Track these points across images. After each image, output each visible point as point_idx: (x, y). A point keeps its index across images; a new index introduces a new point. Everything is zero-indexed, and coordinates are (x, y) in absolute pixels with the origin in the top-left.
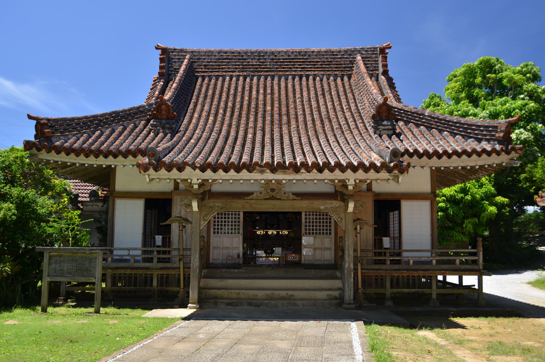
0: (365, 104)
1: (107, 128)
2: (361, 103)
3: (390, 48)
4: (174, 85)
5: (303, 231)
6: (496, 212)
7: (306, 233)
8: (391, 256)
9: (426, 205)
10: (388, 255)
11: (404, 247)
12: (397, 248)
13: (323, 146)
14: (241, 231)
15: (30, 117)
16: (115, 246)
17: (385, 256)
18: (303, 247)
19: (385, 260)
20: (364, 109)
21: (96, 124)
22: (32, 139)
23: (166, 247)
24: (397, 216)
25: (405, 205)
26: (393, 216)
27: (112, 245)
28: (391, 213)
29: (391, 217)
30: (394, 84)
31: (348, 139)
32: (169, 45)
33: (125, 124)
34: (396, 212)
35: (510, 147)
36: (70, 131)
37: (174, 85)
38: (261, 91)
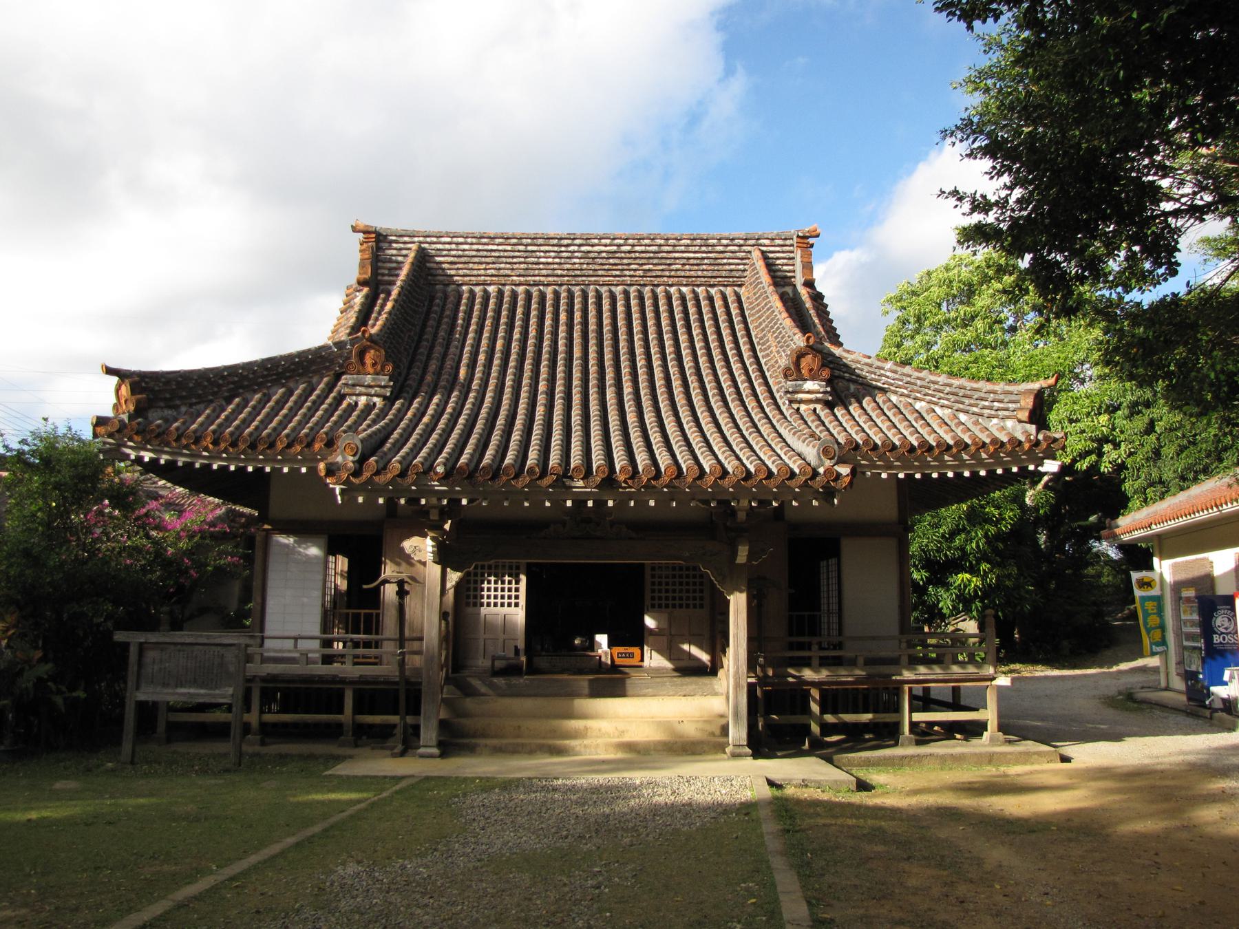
0: (769, 347)
1: (255, 392)
2: (764, 344)
3: (817, 236)
4: (389, 305)
5: (648, 602)
6: (63, 710)
7: (653, 606)
8: (821, 648)
9: (275, 511)
10: (815, 647)
11: (848, 632)
12: (835, 633)
13: (735, 447)
14: (522, 601)
15: (110, 371)
16: (267, 633)
17: (810, 649)
18: (646, 634)
19: (810, 658)
20: (768, 355)
21: (233, 383)
22: (109, 413)
23: (371, 634)
24: (834, 568)
25: (849, 548)
26: (827, 568)
27: (262, 629)
28: (823, 564)
29: (823, 570)
30: (826, 306)
31: (737, 417)
32: (381, 223)
33: (291, 384)
34: (833, 561)
35: (994, 6)
36: (182, 398)
37: (389, 305)
38: (563, 317)
